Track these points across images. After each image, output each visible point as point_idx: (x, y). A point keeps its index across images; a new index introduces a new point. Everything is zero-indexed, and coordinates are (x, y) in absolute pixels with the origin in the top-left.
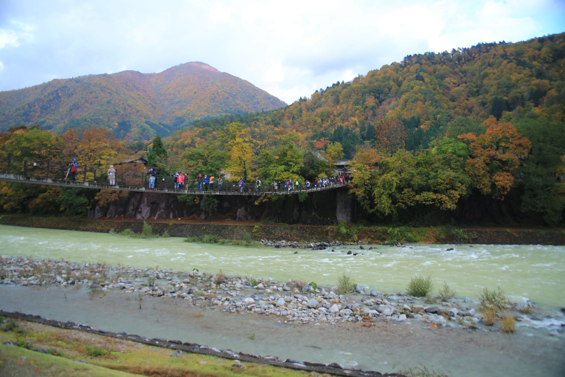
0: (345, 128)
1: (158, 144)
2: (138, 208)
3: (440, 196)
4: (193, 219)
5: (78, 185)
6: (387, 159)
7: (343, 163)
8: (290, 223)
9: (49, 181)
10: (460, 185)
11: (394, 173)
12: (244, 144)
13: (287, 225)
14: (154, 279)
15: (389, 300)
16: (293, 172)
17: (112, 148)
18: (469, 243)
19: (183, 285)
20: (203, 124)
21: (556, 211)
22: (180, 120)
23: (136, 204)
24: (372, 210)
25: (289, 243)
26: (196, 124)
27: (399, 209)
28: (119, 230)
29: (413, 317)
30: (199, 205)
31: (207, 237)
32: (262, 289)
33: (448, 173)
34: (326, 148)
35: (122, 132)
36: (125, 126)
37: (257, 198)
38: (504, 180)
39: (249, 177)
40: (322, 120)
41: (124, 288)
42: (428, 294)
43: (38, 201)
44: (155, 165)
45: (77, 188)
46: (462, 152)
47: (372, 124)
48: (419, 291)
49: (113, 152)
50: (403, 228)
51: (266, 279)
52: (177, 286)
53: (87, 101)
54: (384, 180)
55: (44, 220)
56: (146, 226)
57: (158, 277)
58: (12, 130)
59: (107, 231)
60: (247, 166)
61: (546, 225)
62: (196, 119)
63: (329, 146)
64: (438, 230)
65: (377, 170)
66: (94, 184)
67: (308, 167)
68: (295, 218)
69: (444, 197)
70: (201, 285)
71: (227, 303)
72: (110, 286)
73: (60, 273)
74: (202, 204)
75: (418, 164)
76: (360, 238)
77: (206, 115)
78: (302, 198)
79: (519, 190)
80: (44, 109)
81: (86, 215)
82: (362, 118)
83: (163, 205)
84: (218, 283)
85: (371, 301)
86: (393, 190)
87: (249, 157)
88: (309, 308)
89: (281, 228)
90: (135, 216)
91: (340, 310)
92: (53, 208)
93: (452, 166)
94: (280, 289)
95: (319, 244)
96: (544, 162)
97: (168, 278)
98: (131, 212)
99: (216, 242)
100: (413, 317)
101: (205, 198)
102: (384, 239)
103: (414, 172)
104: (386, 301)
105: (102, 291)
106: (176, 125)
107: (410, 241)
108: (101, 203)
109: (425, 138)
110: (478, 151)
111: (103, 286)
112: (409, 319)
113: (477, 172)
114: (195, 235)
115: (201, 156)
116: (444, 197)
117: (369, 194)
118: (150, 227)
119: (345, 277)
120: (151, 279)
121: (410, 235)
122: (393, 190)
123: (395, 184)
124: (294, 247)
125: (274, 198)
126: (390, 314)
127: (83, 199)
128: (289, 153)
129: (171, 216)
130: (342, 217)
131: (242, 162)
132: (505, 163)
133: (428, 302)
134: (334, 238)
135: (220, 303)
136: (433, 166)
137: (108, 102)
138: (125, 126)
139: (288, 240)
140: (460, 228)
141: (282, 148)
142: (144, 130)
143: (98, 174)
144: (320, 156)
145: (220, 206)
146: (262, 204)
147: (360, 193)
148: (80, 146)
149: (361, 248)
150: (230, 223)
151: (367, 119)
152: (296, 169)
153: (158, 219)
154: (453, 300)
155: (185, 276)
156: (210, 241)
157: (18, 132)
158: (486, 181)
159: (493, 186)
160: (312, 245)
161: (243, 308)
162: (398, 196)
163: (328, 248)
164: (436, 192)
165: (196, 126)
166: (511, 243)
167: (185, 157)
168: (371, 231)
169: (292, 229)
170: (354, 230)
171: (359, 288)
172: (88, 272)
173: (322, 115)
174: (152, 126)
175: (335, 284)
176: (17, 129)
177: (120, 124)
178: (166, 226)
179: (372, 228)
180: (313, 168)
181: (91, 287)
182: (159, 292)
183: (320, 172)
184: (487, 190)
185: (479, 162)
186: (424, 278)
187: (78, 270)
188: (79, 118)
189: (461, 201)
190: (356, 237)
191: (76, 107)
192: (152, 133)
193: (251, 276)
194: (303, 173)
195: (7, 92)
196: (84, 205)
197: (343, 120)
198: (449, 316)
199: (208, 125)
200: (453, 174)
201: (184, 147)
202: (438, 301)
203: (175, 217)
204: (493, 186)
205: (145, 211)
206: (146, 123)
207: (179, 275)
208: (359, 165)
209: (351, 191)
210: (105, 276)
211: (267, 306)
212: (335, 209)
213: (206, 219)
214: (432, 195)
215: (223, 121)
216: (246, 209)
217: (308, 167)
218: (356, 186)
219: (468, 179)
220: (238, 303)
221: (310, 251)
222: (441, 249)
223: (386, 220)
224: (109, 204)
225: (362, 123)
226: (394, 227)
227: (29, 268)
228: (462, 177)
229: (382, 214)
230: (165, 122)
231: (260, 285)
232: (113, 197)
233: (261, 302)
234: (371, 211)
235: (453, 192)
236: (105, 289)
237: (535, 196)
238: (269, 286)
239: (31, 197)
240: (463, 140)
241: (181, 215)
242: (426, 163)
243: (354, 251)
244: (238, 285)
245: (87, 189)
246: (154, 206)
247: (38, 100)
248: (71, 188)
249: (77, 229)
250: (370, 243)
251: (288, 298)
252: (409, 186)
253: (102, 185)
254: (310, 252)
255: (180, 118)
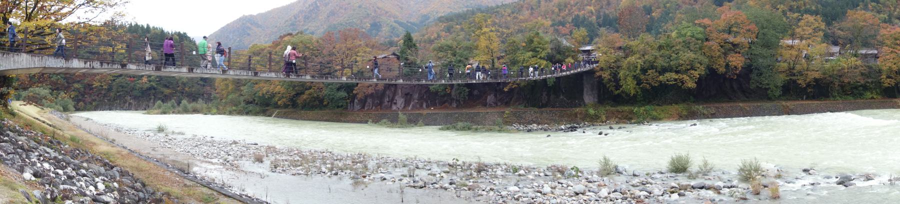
0: (581, 17)
1: (408, 39)
2: (393, 99)
3: (681, 76)
4: (446, 108)
5: (336, 81)
6: (631, 43)
7: (588, 48)
8: (540, 107)
9: (308, 77)
10: (699, 65)
11: (638, 56)
12: (491, 34)
13: (536, 109)
14: (414, 170)
15: (652, 178)
16: (540, 58)
17: (367, 46)
18: (708, 118)
19: (443, 174)
20: (447, 19)
21: (777, 87)
22: (426, 17)
23: (391, 96)
24: (618, 92)
25: (540, 127)
26: (441, 19)
27: (644, 90)
28: (377, 121)
29: (684, 195)
30: (450, 94)
31: (460, 124)
32: (523, 175)
33: (688, 55)
34: (571, 32)
35: (374, 32)
36: (376, 26)
37: (505, 84)
38: (737, 61)
39: (497, 65)
40: (560, 10)
41: (385, 179)
42: (689, 169)
43: (305, 97)
44: (407, 59)
45: (337, 84)
46: (700, 36)
47: (607, 12)
48: (679, 167)
49: (368, 49)
50: (648, 107)
51: (525, 164)
52: (438, 176)
53: (341, 8)
54: (629, 63)
55: (310, 113)
56: (401, 116)
57: (417, 168)
58: (281, 37)
59: (366, 122)
60: (495, 55)
61: (770, 99)
62: (440, 15)
63: (574, 31)
64: (680, 108)
65: (621, 54)
66: (352, 79)
67: (554, 53)
68: (544, 102)
69: (685, 77)
70: (462, 174)
71: (492, 193)
72: (372, 177)
73: (325, 163)
74: (453, 93)
75: (660, 48)
76: (608, 118)
77: (449, 11)
78: (550, 83)
79: (748, 69)
80: (306, 18)
81: (347, 108)
82: (598, 7)
83: (416, 96)
84: (479, 171)
85: (636, 181)
86: (638, 72)
87: (496, 45)
88: (577, 194)
89: (531, 112)
90: (391, 106)
91: (609, 193)
92: (317, 102)
93: (692, 48)
94: (542, 174)
95: (569, 126)
96: (767, 45)
97: (428, 168)
98: (386, 103)
99: (469, 129)
100: (684, 195)
101: (455, 87)
102: (631, 119)
103: (657, 54)
104: (650, 180)
105: (363, 183)
106: (422, 22)
107: (656, 119)
108: (359, 96)
109: (656, 24)
110: (714, 35)
111: (364, 177)
112: (682, 198)
113: (713, 54)
114: (449, 124)
115: (450, 47)
116: (685, 77)
117: (615, 76)
118: (405, 116)
119: (605, 159)
120: (411, 167)
121: (654, 113)
122: (638, 72)
123: (639, 66)
124: (545, 130)
125: (522, 84)
126: (661, 193)
127: (343, 94)
128: (535, 39)
129: (424, 106)
130: (589, 98)
131: (490, 51)
132: (735, 45)
133: (691, 177)
134: (583, 119)
135: (484, 193)
136: (674, 49)
137: (360, 7)
138: (376, 26)
139: (539, 124)
140: (699, 105)
141: (527, 35)
142: (394, 29)
143: (355, 70)
144: (565, 43)
145: (470, 94)
146: (511, 90)
147: (606, 75)
148: (337, 46)
149: (611, 128)
150: (482, 110)
151: (602, 7)
152: (543, 54)
153: (412, 109)
154: (713, 173)
155: (444, 165)
156: (463, 129)
157: (286, 39)
158: (722, 62)
159: (727, 66)
160: (563, 127)
161: (509, 197)
162: (642, 77)
163: (579, 130)
164: (677, 72)
165: (441, 21)
166: (744, 116)
167: (434, 50)
168: (618, 111)
169: (542, 113)
170: (602, 111)
171: (621, 170)
172: (349, 162)
173: (559, 5)
174: (400, 24)
175: (596, 166)
176: (285, 36)
177: (372, 25)
178: (421, 115)
179: (620, 108)
180: (559, 53)
181: (353, 178)
182: (421, 183)
183: (568, 56)
184: (722, 70)
185: (714, 45)
186: (683, 154)
187: (340, 160)
188: (335, 22)
189: (699, 82)
190: (604, 118)
191: (333, 13)
192: (402, 32)
193: (509, 162)
194: (551, 59)
195: (278, 9)
196: (344, 99)
197: (580, 10)
198: (717, 190)
199: (452, 20)
200: (692, 55)
201: (431, 42)
202: (700, 175)
203: (428, 107)
204: (727, 66)
205: (400, 101)
206: (395, 22)
207: (438, 163)
208: (605, 49)
209: (598, 74)
210: (366, 167)
211: (533, 195)
212: (581, 92)
213: (457, 107)
214: (674, 76)
215: (466, 15)
216: (496, 96)
217: (554, 53)
218: (602, 69)
219: (707, 60)
220: (504, 193)
221: (561, 134)
222: (686, 125)
223: (631, 100)
224: (366, 97)
225: (598, 11)
226: (639, 107)
227: (298, 158)
228: (701, 58)
229: (628, 95)
230: (412, 20)
231: (522, 172)
232: (370, 91)
233: (526, 190)
234: (617, 92)
235: (693, 72)
236: (366, 180)
237: (761, 74)
238: (529, 172)
239: (298, 94)
240: (700, 25)
241: (434, 105)
242: (668, 46)
243: (604, 131)
244: (499, 172)
245: (347, 84)
246: (408, 97)
247: (301, 12)
248: (332, 84)
249: (339, 121)
250: (617, 123)
251: (554, 184)
252: (652, 67)
253: (360, 79)
254: (561, 134)
255: (425, 16)
